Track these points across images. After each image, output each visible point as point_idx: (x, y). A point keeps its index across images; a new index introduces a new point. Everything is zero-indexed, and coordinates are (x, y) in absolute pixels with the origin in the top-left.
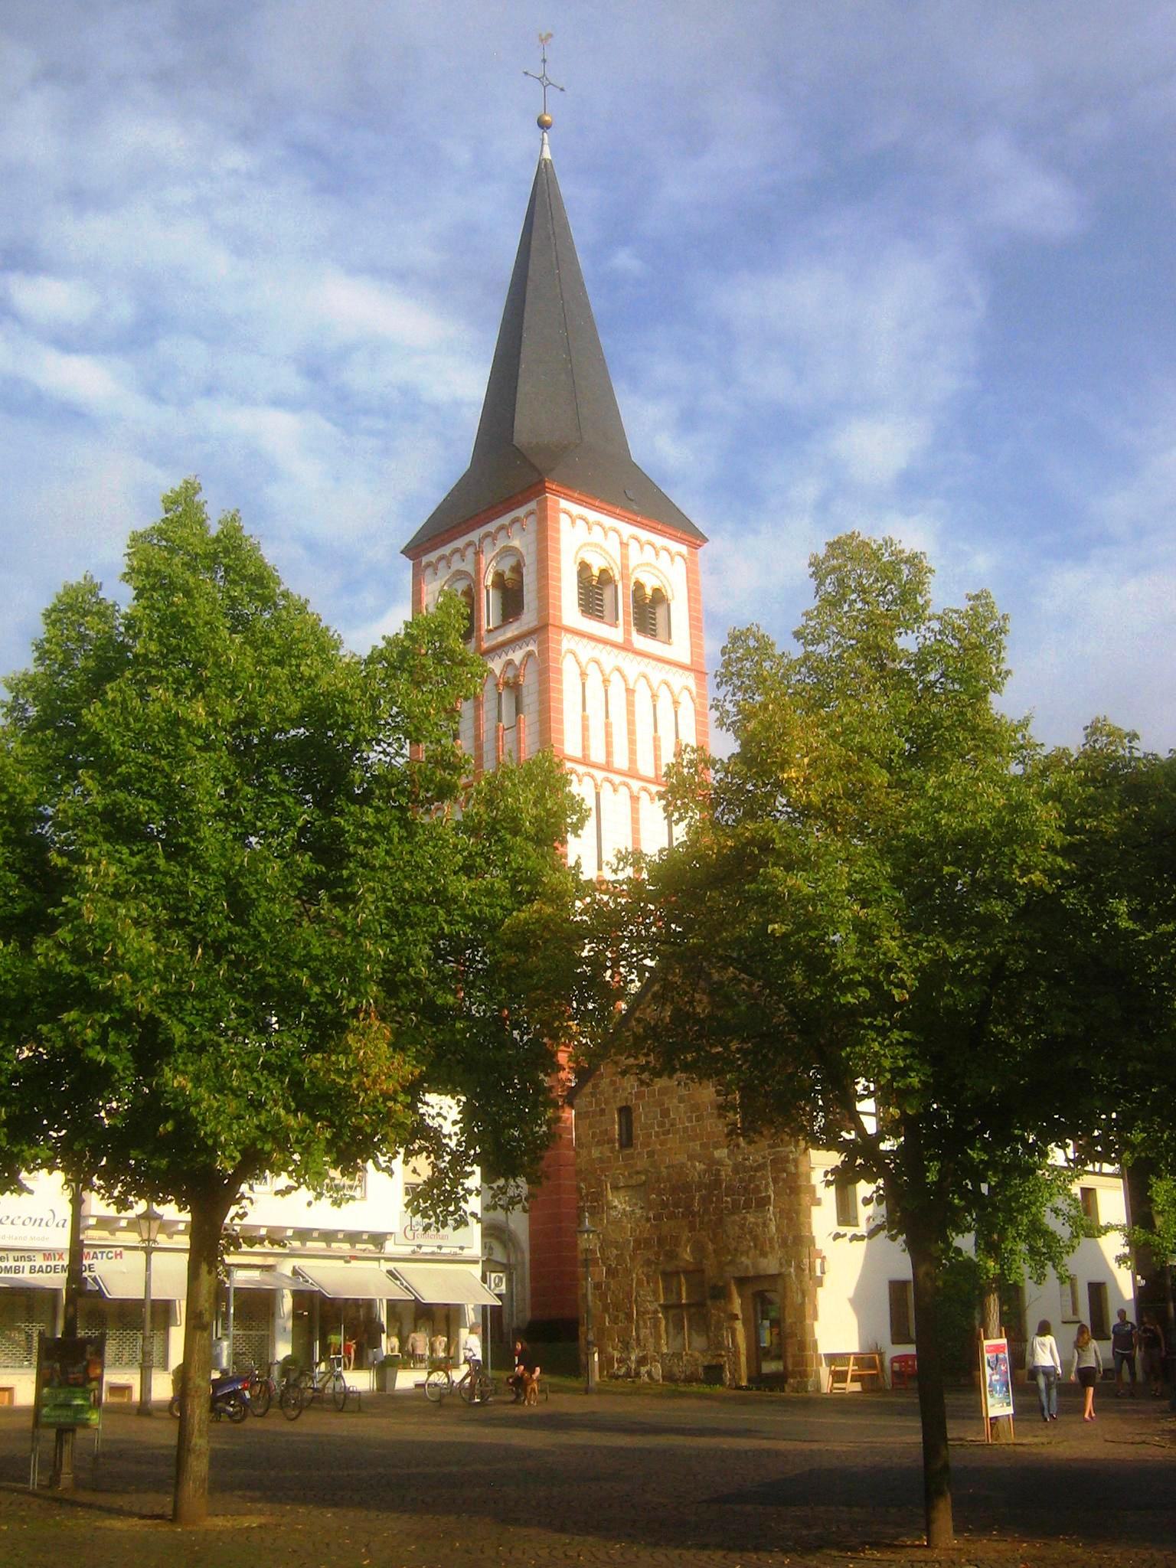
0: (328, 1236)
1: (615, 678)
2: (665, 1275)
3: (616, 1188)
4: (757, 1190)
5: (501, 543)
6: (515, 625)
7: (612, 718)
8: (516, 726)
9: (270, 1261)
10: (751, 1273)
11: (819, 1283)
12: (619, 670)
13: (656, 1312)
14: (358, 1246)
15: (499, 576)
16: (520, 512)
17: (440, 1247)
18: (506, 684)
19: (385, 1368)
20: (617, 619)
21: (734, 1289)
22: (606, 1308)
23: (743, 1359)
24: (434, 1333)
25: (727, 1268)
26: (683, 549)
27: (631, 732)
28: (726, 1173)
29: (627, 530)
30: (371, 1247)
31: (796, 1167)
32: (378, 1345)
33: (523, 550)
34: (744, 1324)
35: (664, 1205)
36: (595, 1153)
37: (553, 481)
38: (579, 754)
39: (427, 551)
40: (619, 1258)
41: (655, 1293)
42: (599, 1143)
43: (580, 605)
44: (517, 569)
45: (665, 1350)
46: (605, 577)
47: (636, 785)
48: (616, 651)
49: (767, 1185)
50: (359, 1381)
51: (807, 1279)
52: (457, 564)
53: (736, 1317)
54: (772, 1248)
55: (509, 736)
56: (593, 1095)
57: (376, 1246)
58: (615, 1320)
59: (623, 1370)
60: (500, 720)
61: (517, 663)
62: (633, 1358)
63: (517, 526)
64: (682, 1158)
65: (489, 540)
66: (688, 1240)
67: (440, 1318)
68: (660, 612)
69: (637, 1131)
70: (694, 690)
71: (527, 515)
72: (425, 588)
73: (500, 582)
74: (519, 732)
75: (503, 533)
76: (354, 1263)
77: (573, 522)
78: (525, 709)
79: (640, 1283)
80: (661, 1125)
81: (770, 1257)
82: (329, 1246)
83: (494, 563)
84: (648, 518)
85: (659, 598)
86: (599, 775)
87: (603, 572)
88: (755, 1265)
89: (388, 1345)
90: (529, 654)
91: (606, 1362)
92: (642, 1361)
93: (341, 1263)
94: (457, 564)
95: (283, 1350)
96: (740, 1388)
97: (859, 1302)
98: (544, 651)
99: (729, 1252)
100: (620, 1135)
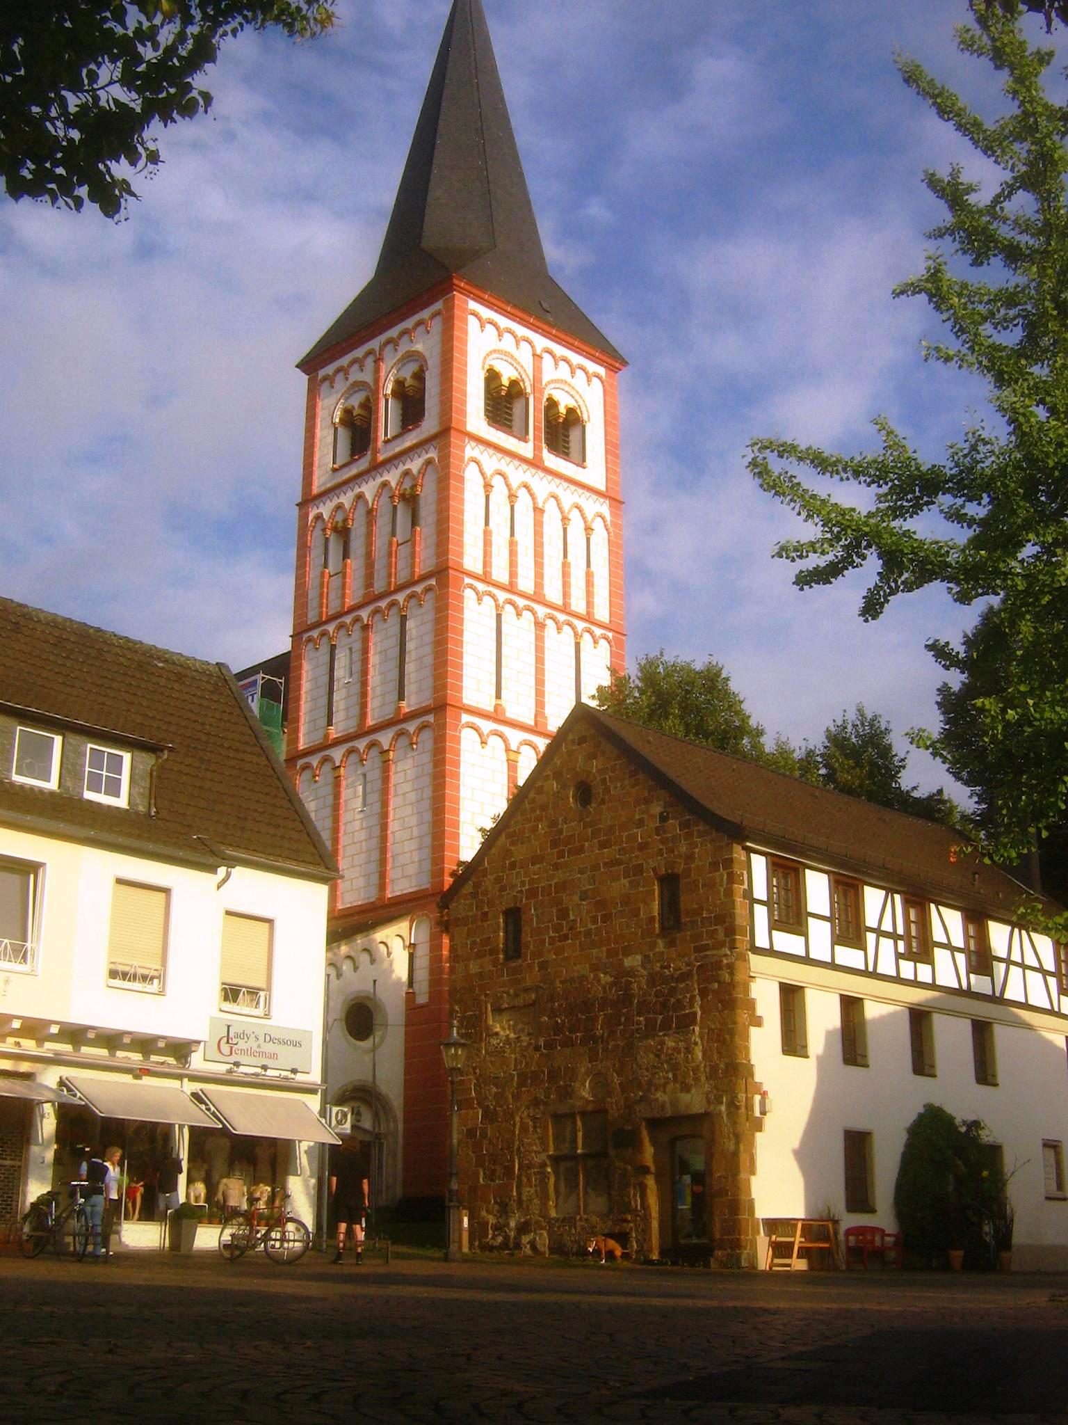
0: (111, 1040)
2: (558, 1118)
3: (498, 1010)
4: (679, 1005)
5: (404, 347)
6: (414, 433)
7: (517, 536)
8: (411, 541)
9: (25, 1067)
10: (669, 1113)
11: (758, 1126)
12: (526, 486)
13: (544, 1165)
14: (154, 1058)
15: (399, 383)
16: (425, 314)
17: (265, 1068)
18: (403, 497)
19: (182, 1221)
20: (527, 433)
21: (645, 1134)
22: (480, 1163)
23: (655, 1224)
24: (255, 1181)
25: (637, 1108)
26: (601, 371)
28: (638, 986)
29: (541, 342)
30: (171, 1060)
31: (732, 974)
32: (173, 1187)
33: (427, 356)
34: (658, 1182)
35: (558, 1029)
36: (474, 968)
37: (462, 279)
38: (478, 569)
39: (325, 363)
40: (499, 1097)
41: (543, 1140)
42: (480, 955)
43: (488, 417)
44: (420, 376)
45: (553, 1214)
46: (514, 391)
47: (541, 611)
48: (525, 467)
49: (693, 998)
50: (141, 1236)
51: (742, 1119)
52: (356, 375)
53: (646, 1170)
54: (697, 1079)
55: (404, 551)
56: (474, 895)
57: (178, 1059)
58: (491, 1176)
59: (500, 1239)
60: (393, 534)
61: (415, 471)
62: (512, 1224)
63: (421, 329)
64: (582, 969)
65: (390, 347)
66: (587, 1073)
67: (264, 1158)
68: (574, 435)
69: (527, 937)
70: (608, 518)
71: (434, 316)
72: (320, 404)
73: (400, 392)
74: (414, 545)
75: (406, 338)
76: (147, 1081)
77: (482, 326)
78: (422, 522)
79: (524, 1129)
80: (558, 928)
81: (693, 1091)
82: (112, 1054)
83: (394, 371)
84: (565, 332)
85: (573, 420)
86: (502, 596)
87: (514, 383)
88: (674, 1103)
89: (185, 1191)
90: (429, 462)
91: (478, 1229)
92: (523, 1228)
93: (127, 1078)
94: (356, 375)
95: (36, 1189)
96: (652, 1262)
97: (806, 1156)
98: (445, 457)
99: (640, 1087)
100: (506, 944)
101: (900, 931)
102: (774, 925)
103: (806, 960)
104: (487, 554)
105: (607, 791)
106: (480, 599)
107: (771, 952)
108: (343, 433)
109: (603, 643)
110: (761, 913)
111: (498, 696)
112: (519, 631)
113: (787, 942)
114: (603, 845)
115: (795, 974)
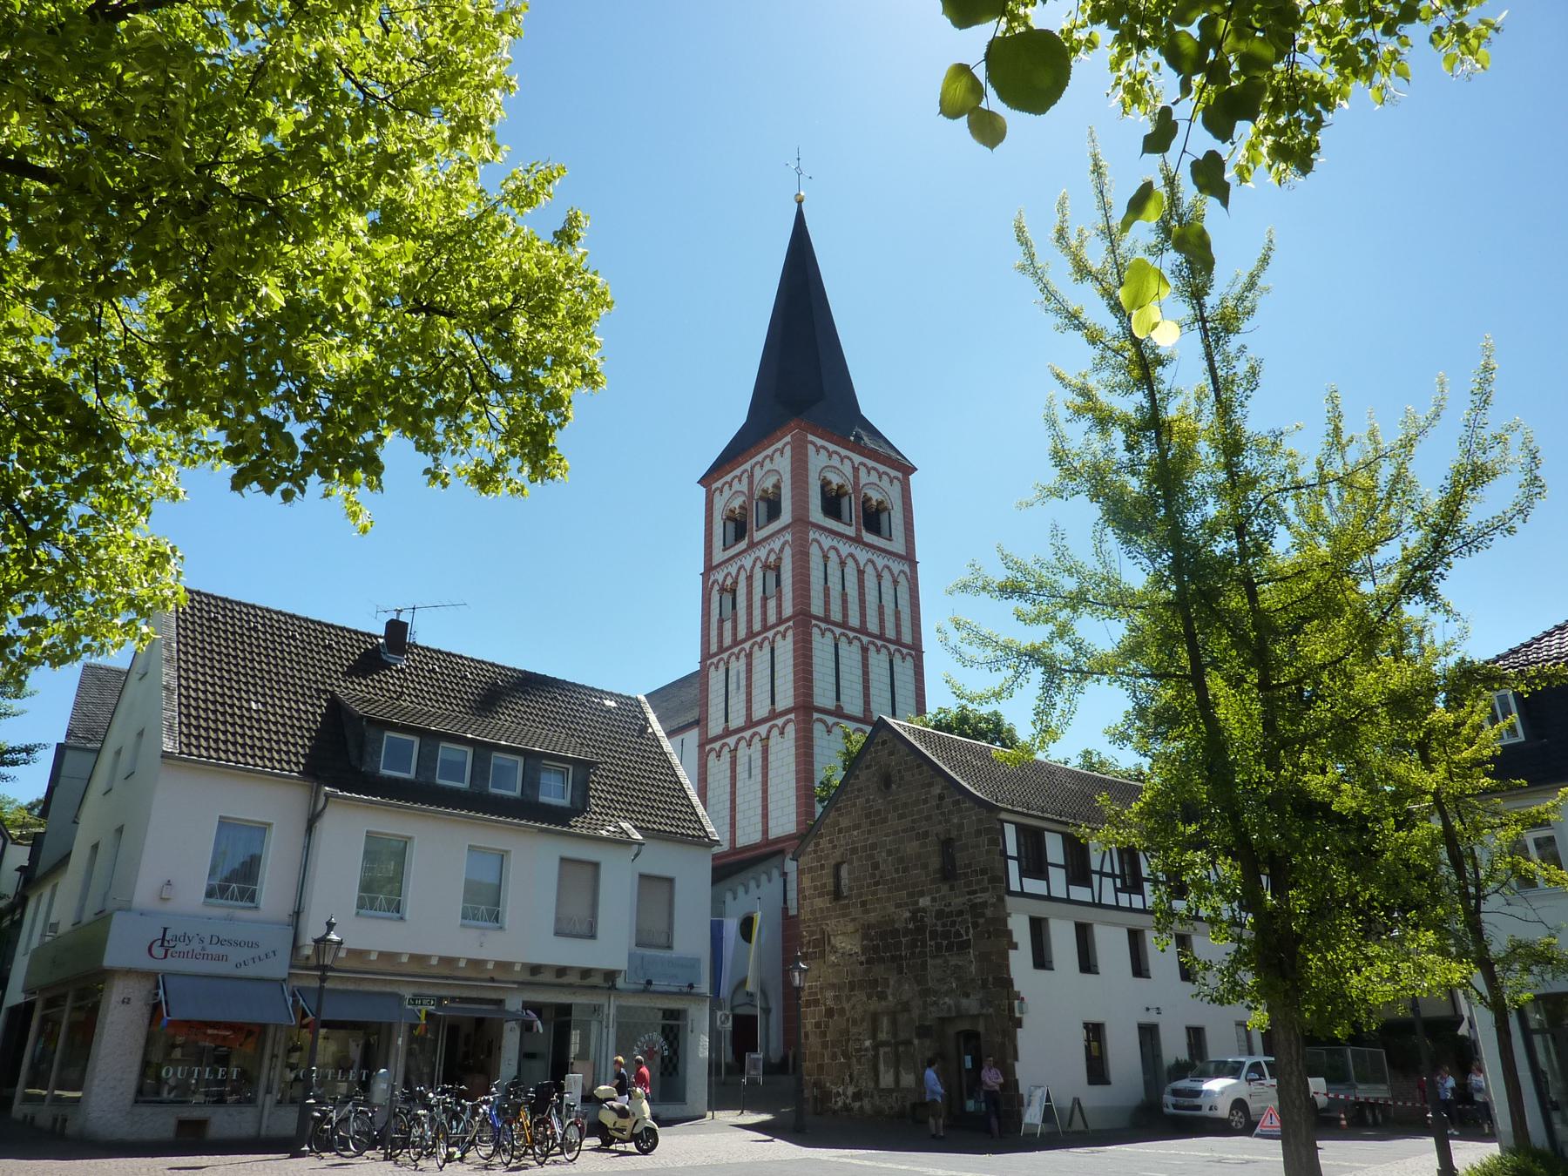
1: (850, 562)
27: (862, 602)
38: (821, 613)
44: (777, 486)
47: (865, 639)
52: (736, 486)
56: (815, 852)
68: (884, 517)
80: (873, 876)
86: (838, 631)
87: (840, 487)
101: (1117, 872)
102: (1024, 873)
103: (1049, 898)
104: (827, 603)
105: (902, 778)
106: (823, 635)
107: (1022, 894)
108: (731, 526)
109: (909, 659)
110: (1013, 867)
111: (838, 699)
112: (851, 656)
113: (1034, 886)
114: (901, 817)
115: (1040, 909)
